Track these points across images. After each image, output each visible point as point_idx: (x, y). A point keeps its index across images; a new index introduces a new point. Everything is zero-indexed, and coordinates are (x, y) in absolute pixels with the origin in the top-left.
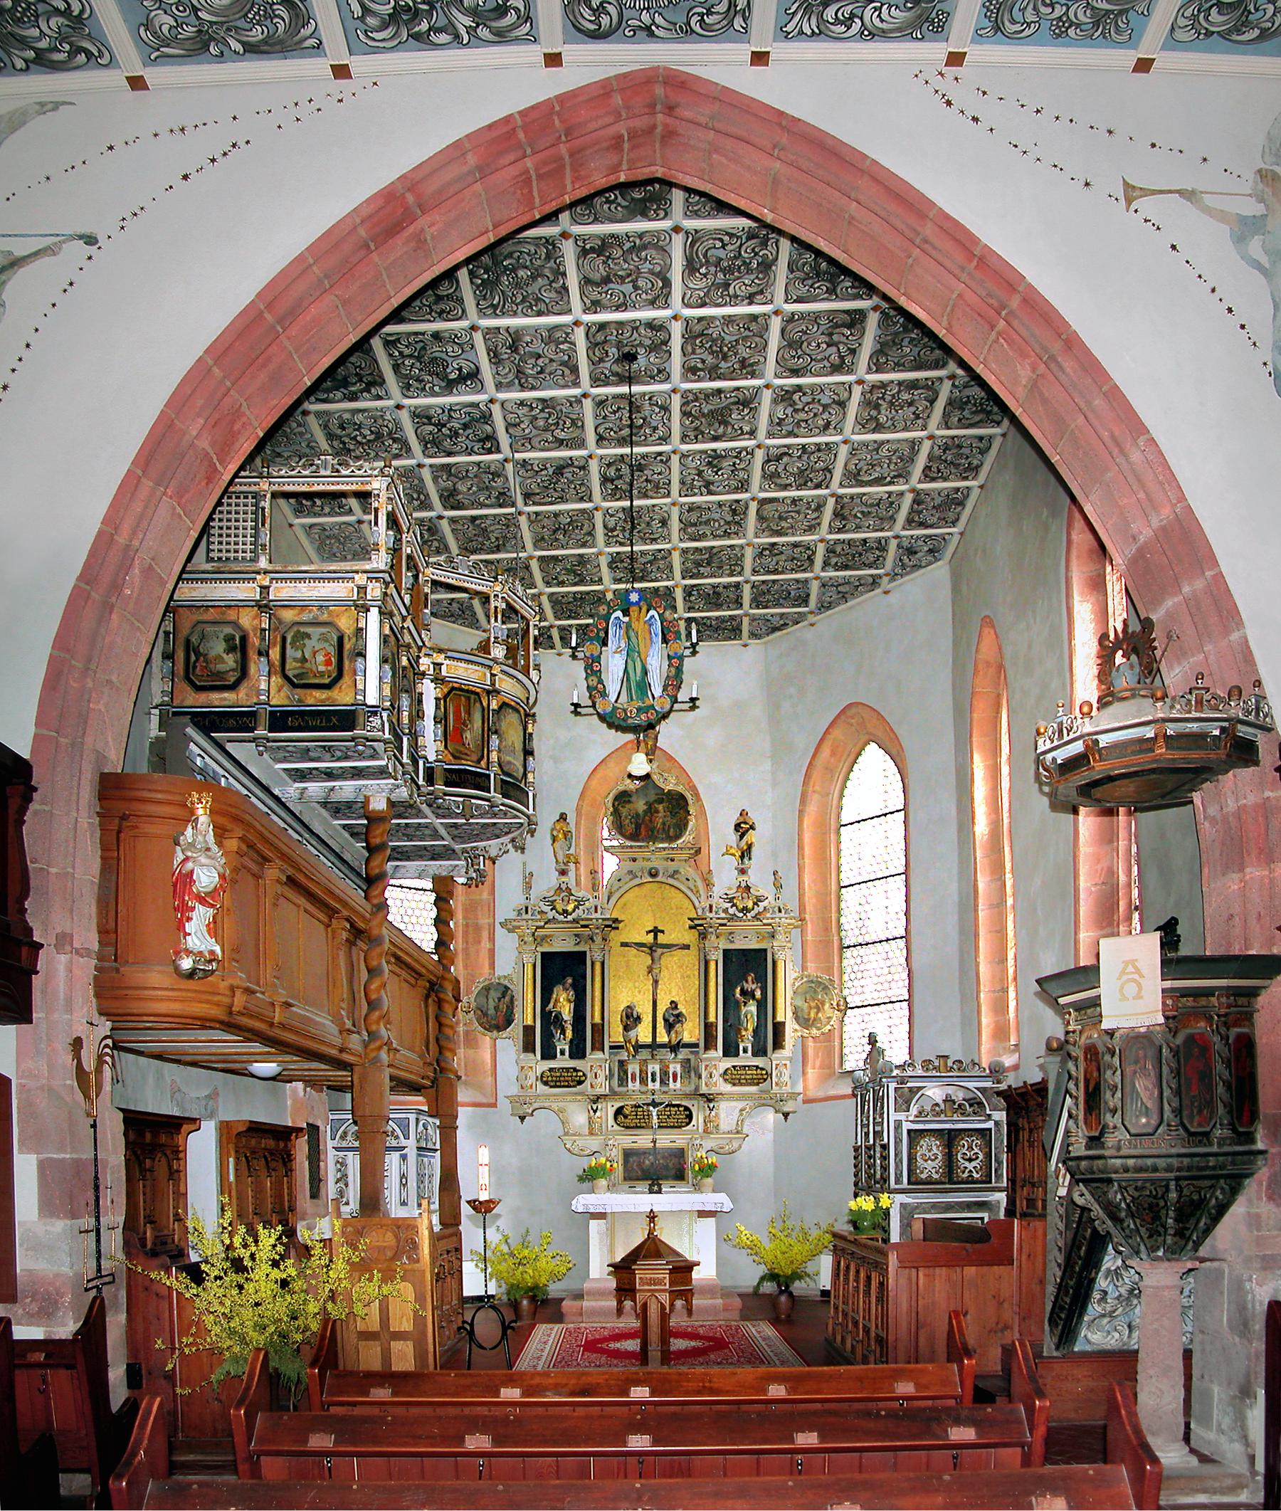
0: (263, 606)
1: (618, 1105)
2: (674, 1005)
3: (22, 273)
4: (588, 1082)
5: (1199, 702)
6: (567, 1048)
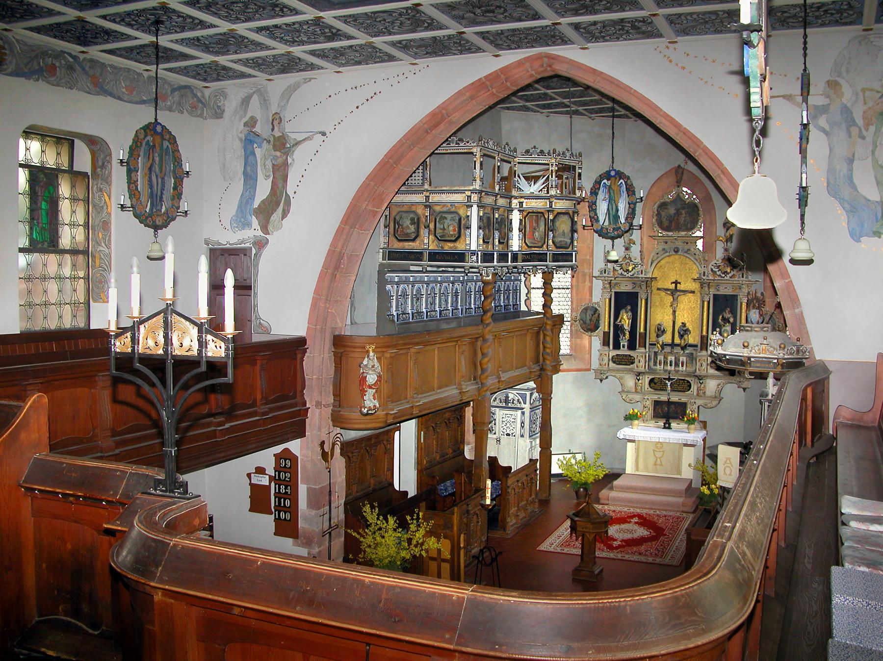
0: (428, 206)
1: (651, 377)
2: (684, 324)
3: (300, 148)
4: (635, 365)
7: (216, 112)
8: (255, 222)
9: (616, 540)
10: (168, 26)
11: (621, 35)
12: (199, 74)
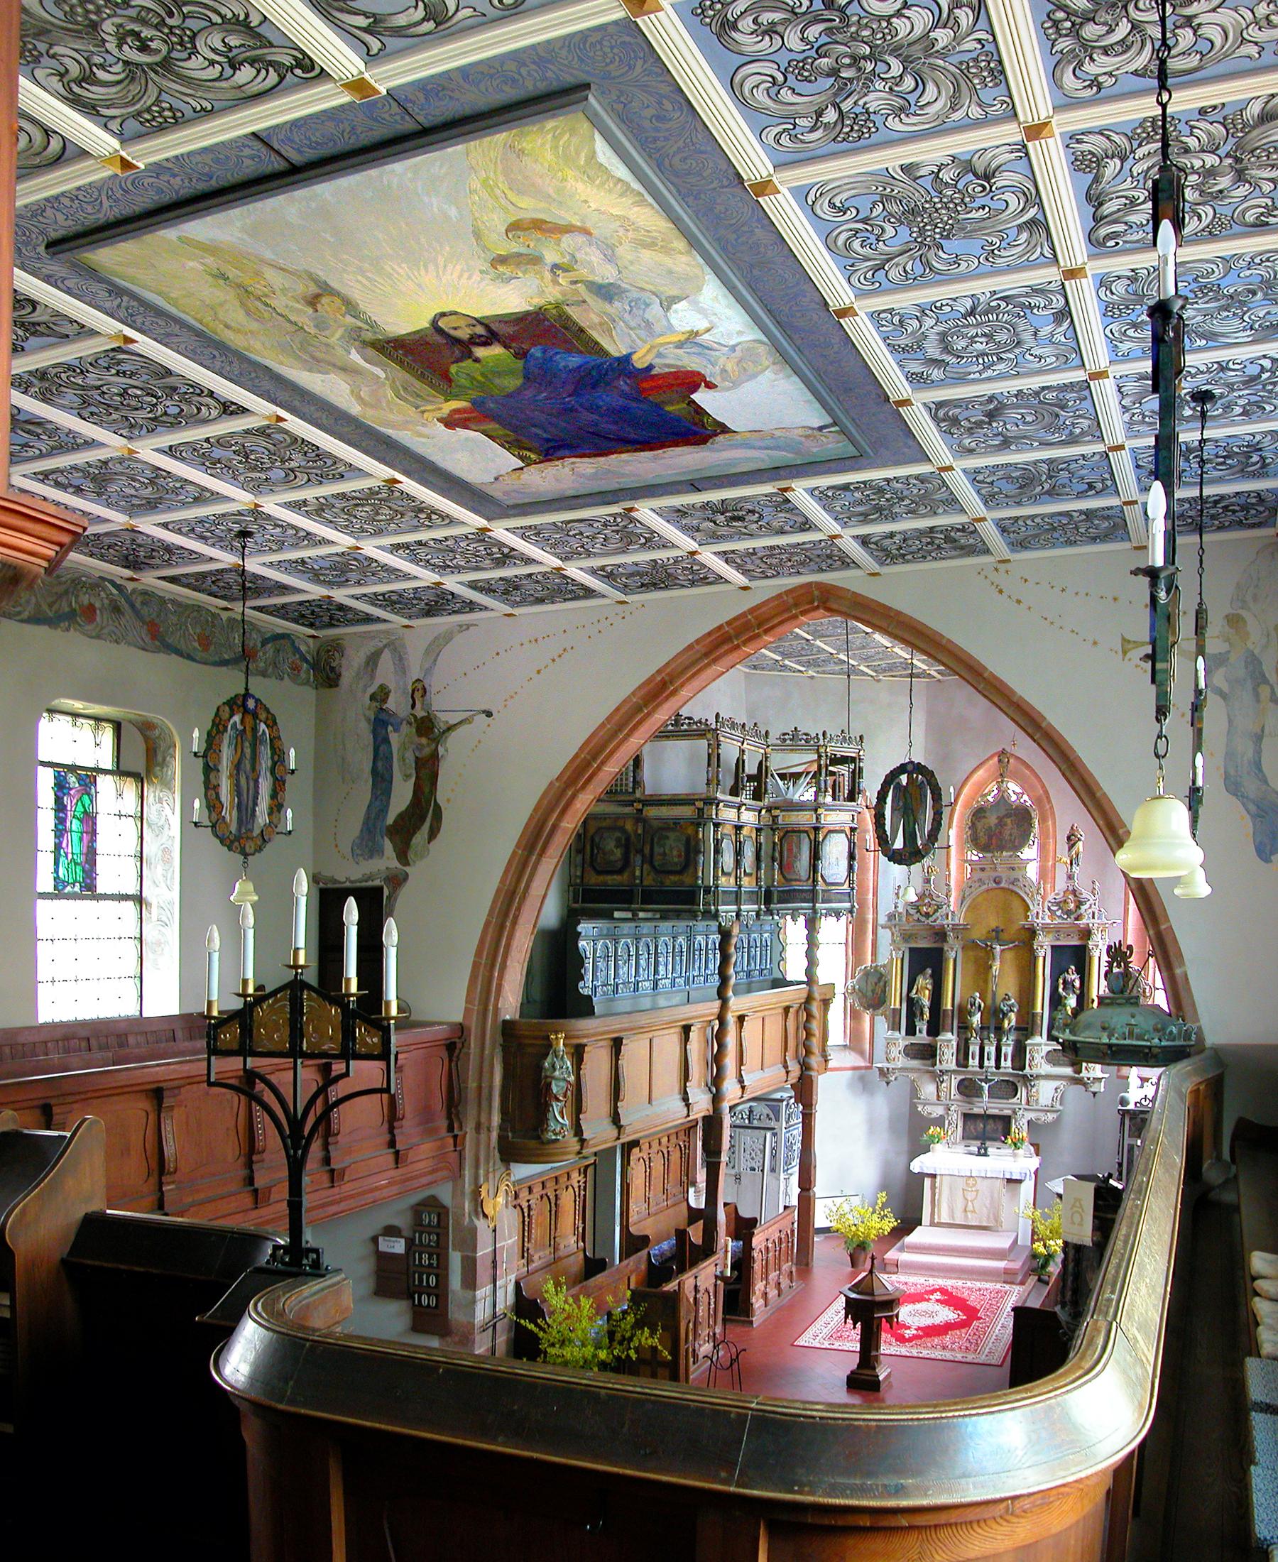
5: (1131, 1033)
6: (925, 1028)
7: (328, 678)
8: (388, 846)
9: (909, 1328)
10: (259, 542)
11: (930, 552)
12: (303, 616)
